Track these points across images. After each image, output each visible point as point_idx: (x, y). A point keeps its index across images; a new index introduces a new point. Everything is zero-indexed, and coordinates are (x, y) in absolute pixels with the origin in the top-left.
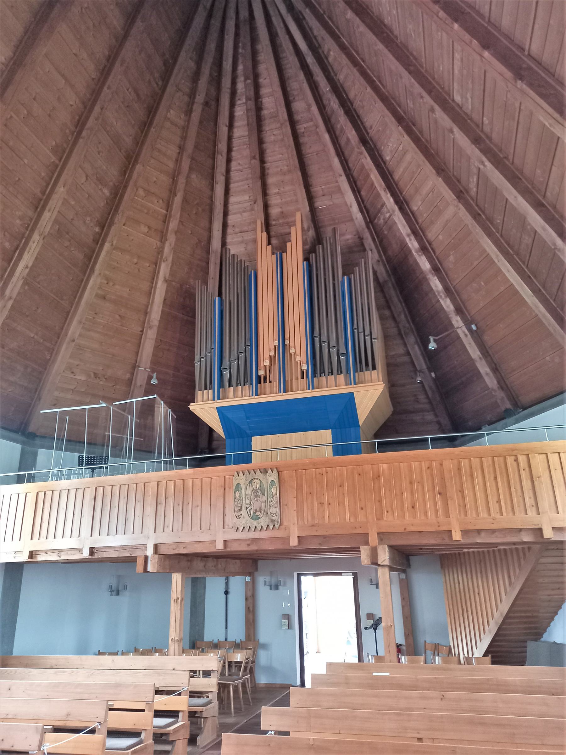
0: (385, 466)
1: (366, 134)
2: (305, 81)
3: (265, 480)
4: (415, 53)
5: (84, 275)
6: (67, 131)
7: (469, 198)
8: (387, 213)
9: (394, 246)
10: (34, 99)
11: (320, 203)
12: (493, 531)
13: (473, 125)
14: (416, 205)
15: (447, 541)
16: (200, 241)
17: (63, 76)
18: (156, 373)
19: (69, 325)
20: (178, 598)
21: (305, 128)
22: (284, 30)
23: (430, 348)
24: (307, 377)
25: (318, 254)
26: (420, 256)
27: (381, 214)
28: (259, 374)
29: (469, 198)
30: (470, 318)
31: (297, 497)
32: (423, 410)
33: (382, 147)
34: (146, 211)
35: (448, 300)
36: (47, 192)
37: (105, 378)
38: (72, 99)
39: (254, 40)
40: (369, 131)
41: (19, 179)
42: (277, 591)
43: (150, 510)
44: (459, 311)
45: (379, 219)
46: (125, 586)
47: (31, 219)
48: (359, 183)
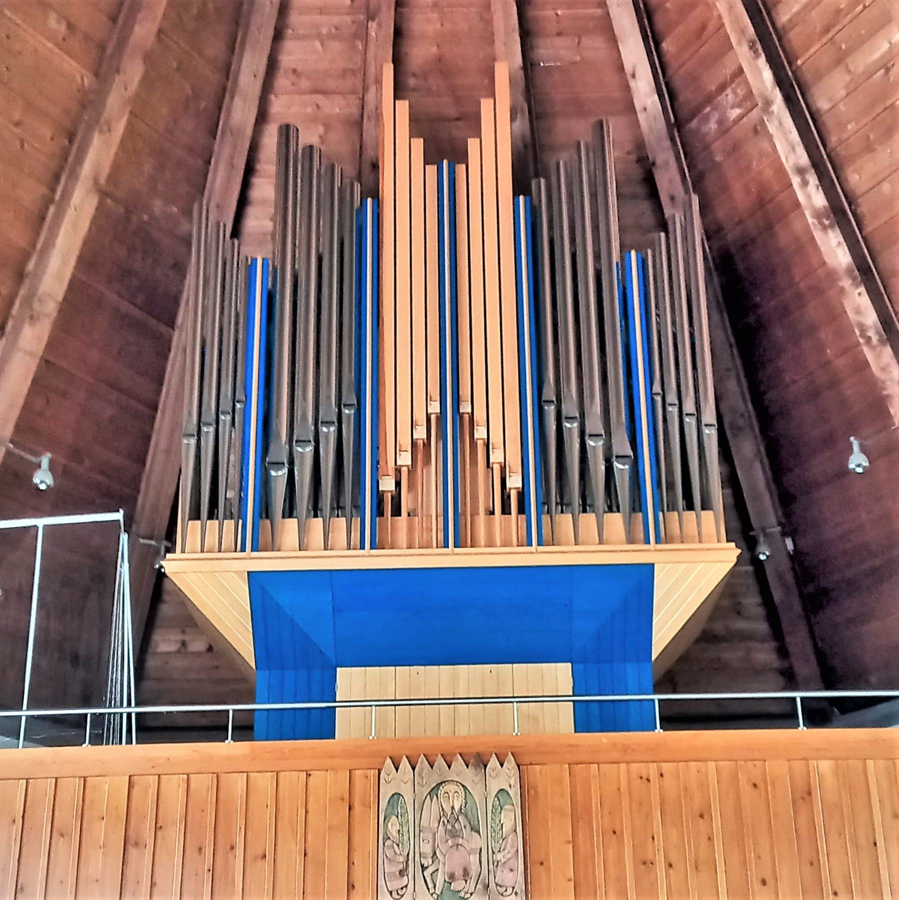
0: (825, 766)
3: (480, 786)
8: (732, 108)
18: (49, 455)
23: (852, 466)
26: (825, 228)
27: (714, 109)
28: (380, 489)
32: (746, 637)
45: (706, 119)
48: (660, 21)
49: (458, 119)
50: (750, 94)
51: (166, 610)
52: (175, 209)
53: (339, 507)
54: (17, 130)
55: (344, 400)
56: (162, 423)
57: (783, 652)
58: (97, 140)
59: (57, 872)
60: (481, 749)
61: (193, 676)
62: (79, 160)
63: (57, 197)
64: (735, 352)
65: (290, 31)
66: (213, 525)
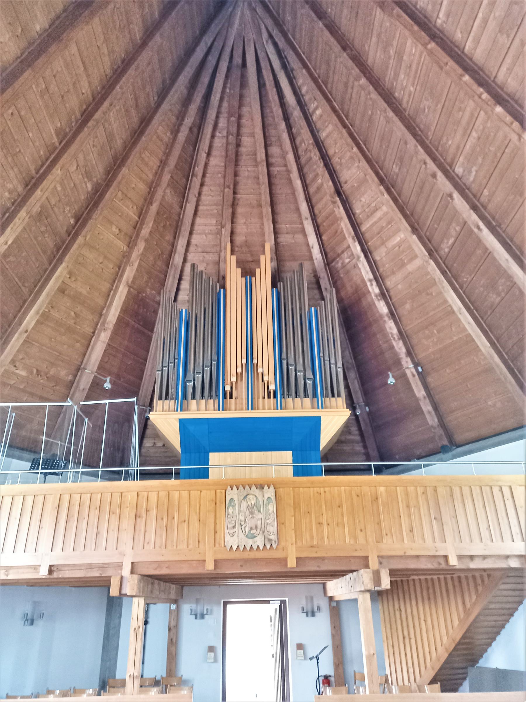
0: (382, 489)
1: (340, 188)
2: (286, 131)
3: (261, 496)
4: (422, 126)
6: (73, 117)
7: (438, 257)
8: (347, 258)
9: (349, 288)
10: (55, 76)
11: (284, 239)
12: (485, 557)
13: (470, 194)
14: (379, 255)
15: (443, 566)
16: (162, 253)
17: (83, 63)
20: (139, 627)
21: (278, 171)
24: (275, 397)
26: (379, 300)
27: (341, 259)
29: (438, 257)
30: (417, 361)
31: (294, 516)
32: (353, 441)
33: (354, 201)
35: (401, 343)
36: (41, 171)
37: (47, 377)
38: (85, 88)
39: (243, 84)
40: (343, 185)
41: (20, 151)
43: (127, 524)
44: (409, 353)
45: (338, 262)
47: (19, 195)
48: (322, 229)
49: (252, 262)
50: (352, 254)
51: (148, 432)
52: (154, 292)
53: (211, 396)
54: (101, 265)
55: (213, 359)
56: (149, 365)
57: (365, 447)
58: (128, 268)
59: (112, 527)
60: (262, 482)
61: (157, 455)
62: (122, 276)
63: (114, 288)
64: (348, 341)
65: (195, 232)
66: (167, 402)
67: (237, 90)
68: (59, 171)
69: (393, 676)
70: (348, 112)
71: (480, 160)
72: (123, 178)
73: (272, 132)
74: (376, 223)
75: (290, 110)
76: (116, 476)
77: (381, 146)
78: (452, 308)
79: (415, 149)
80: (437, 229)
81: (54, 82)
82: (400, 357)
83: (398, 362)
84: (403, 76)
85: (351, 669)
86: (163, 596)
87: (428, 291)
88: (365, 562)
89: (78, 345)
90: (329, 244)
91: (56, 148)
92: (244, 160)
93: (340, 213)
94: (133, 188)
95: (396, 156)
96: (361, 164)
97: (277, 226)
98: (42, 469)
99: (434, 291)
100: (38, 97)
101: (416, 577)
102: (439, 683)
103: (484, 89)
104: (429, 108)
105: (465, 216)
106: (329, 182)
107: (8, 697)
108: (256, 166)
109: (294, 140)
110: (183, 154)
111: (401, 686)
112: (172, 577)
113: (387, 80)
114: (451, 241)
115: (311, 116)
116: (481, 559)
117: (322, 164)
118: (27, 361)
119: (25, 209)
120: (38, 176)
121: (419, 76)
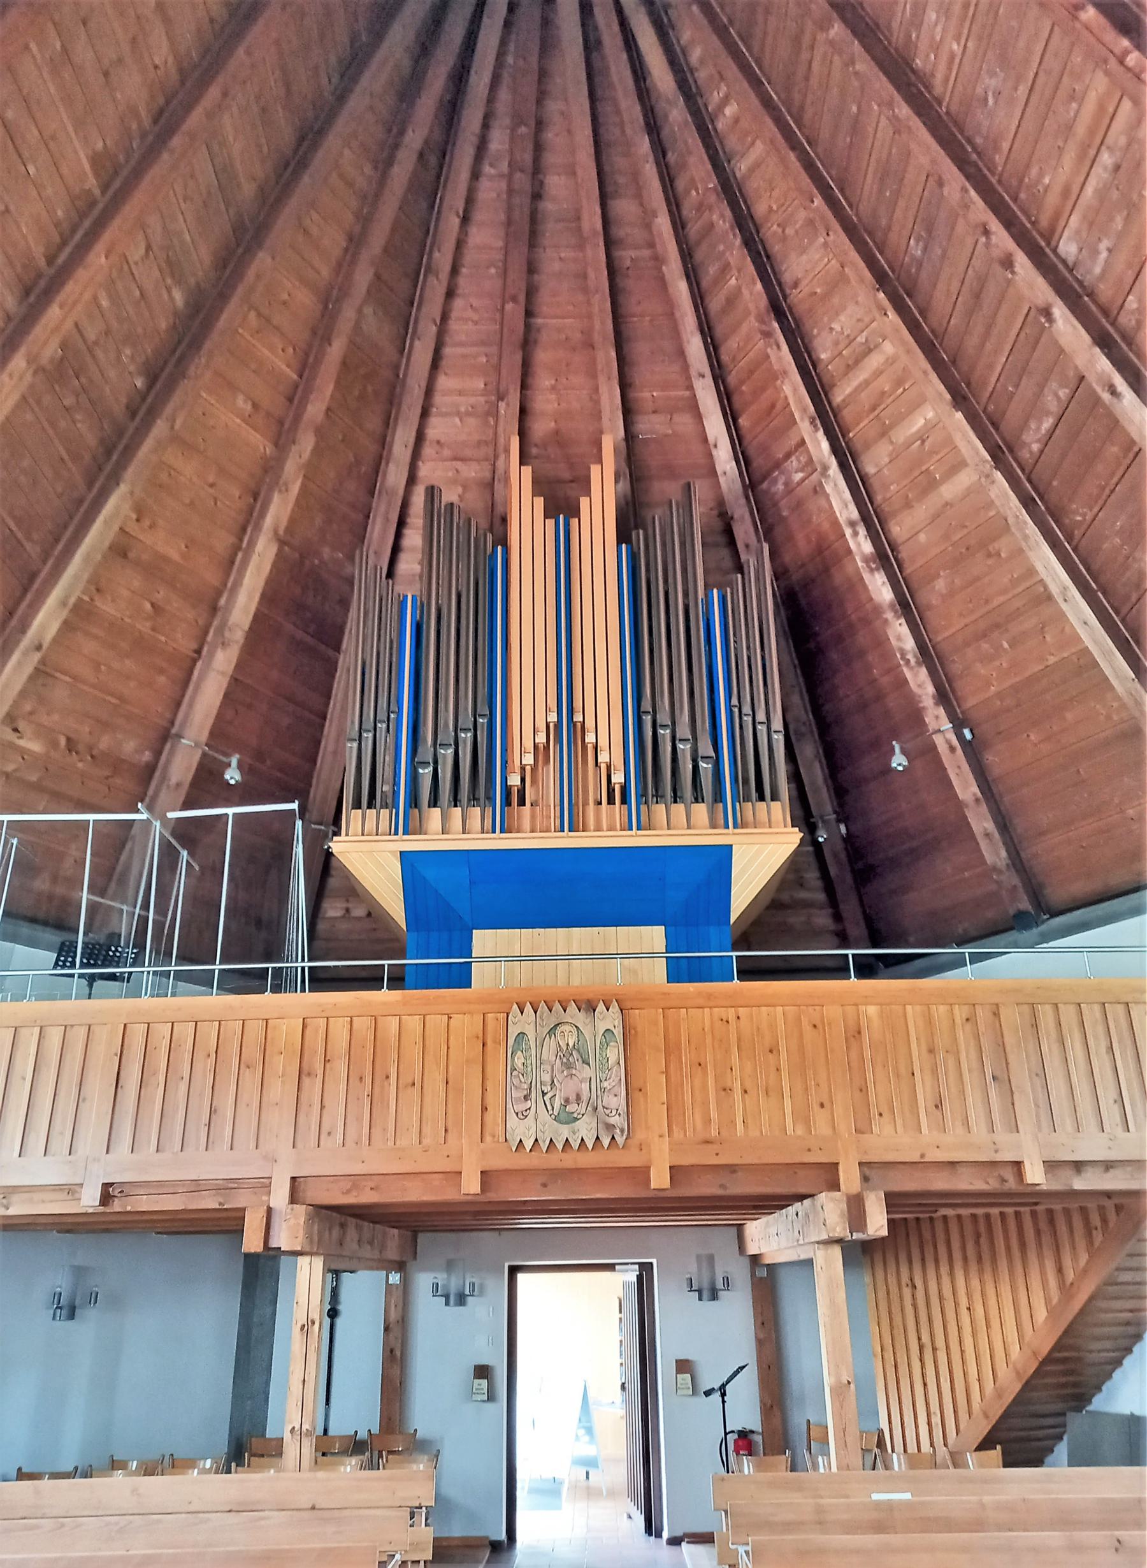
0: (872, 1010)
2: (651, 158)
3: (590, 1027)
4: (979, 140)
5: (90, 485)
6: (134, 126)
11: (649, 425)
12: (1108, 1165)
13: (1094, 308)
14: (875, 461)
15: (1012, 1184)
16: (358, 462)
18: (237, 756)
19: (34, 607)
20: (313, 1323)
22: (619, 41)
23: (894, 765)
24: (625, 800)
25: (650, 532)
26: (872, 570)
27: (782, 473)
30: (960, 716)
31: (667, 1072)
32: (807, 905)
33: (815, 331)
34: (253, 366)
35: (923, 672)
36: (60, 260)
37: (92, 757)
38: (161, 53)
39: (547, 44)
40: (788, 291)
42: (461, 1308)
43: (281, 1090)
44: (943, 697)
45: (775, 481)
46: (93, 1295)
48: (737, 401)
49: (572, 481)
50: (811, 460)
51: (333, 882)
52: (341, 555)
54: (211, 491)
56: (330, 730)
57: (838, 917)
58: (276, 498)
60: (591, 996)
62: (262, 515)
64: (799, 671)
65: (434, 410)
66: (371, 813)
67: (534, 59)
68: (103, 259)
69: (894, 1432)
70: (802, 108)
71: (1119, 222)
72: (258, 277)
73: (617, 161)
74: (867, 383)
75: (661, 106)
76: (252, 983)
77: (881, 191)
78: (1046, 587)
79: (962, 198)
80: (1013, 394)
81: (83, 37)
82: (921, 705)
83: (916, 717)
84: (934, 16)
85: (798, 1420)
86: (367, 1252)
87: (991, 548)
88: (829, 1176)
89: (162, 680)
90: (754, 438)
91: (93, 204)
92: (551, 230)
93: (780, 359)
94: (284, 303)
95: (916, 217)
96: (832, 237)
97: (633, 394)
98: (83, 965)
99: (1003, 546)
100: (46, 75)
101: (950, 1212)
102: (999, 1447)
103: (1131, 39)
104: (998, 94)
105: (1080, 361)
106: (755, 284)
107: (21, 1475)
108: (581, 246)
109: (672, 181)
110: (403, 218)
111: (913, 1454)
112: (392, 1210)
113: (895, 25)
114: (1047, 424)
115: (712, 122)
116: (1099, 1170)
117: (738, 241)
118: (44, 720)
119: (23, 350)
120: (52, 271)
121: (974, 15)
